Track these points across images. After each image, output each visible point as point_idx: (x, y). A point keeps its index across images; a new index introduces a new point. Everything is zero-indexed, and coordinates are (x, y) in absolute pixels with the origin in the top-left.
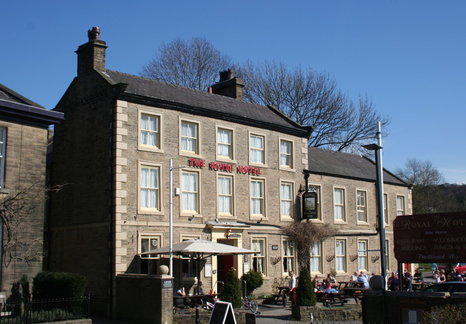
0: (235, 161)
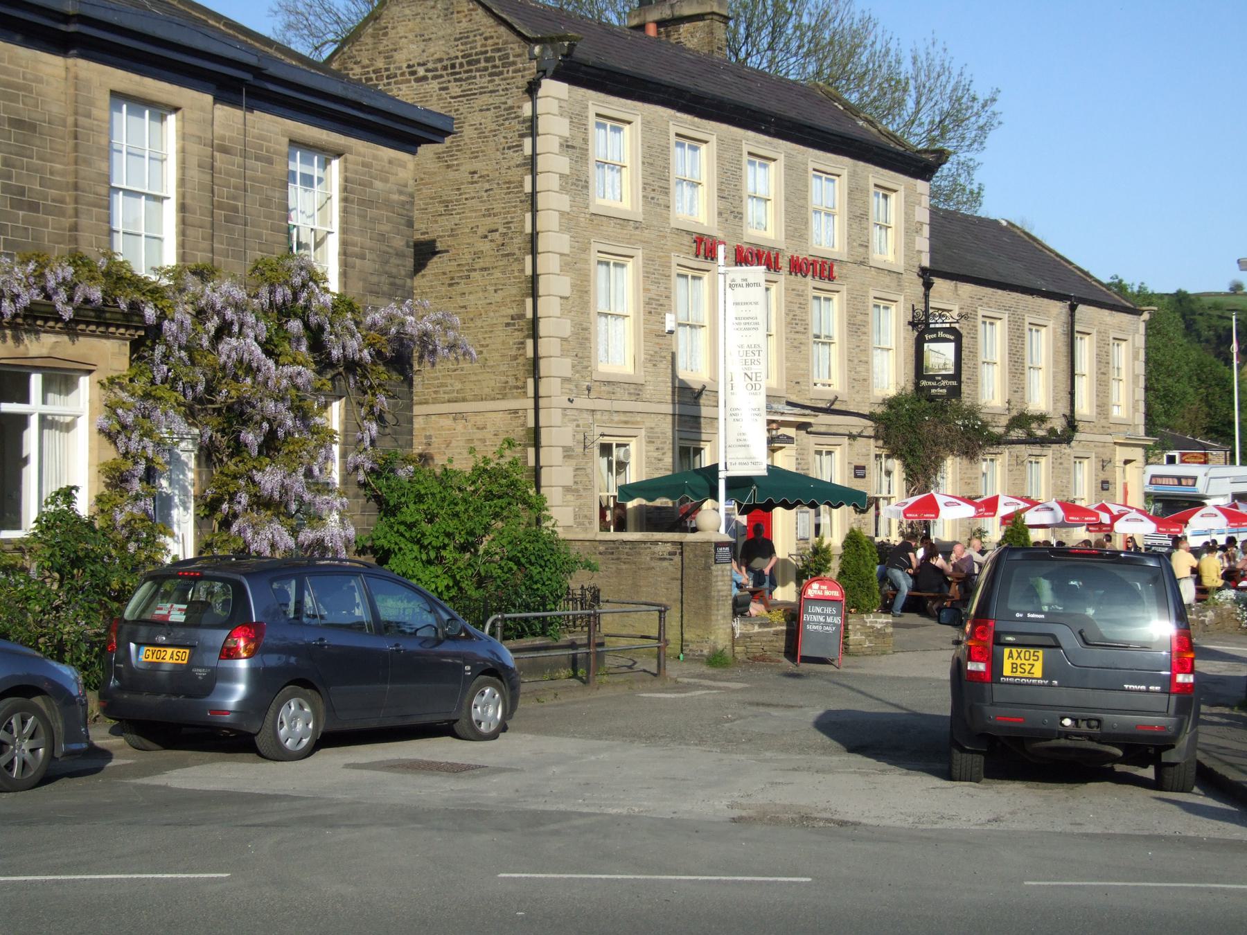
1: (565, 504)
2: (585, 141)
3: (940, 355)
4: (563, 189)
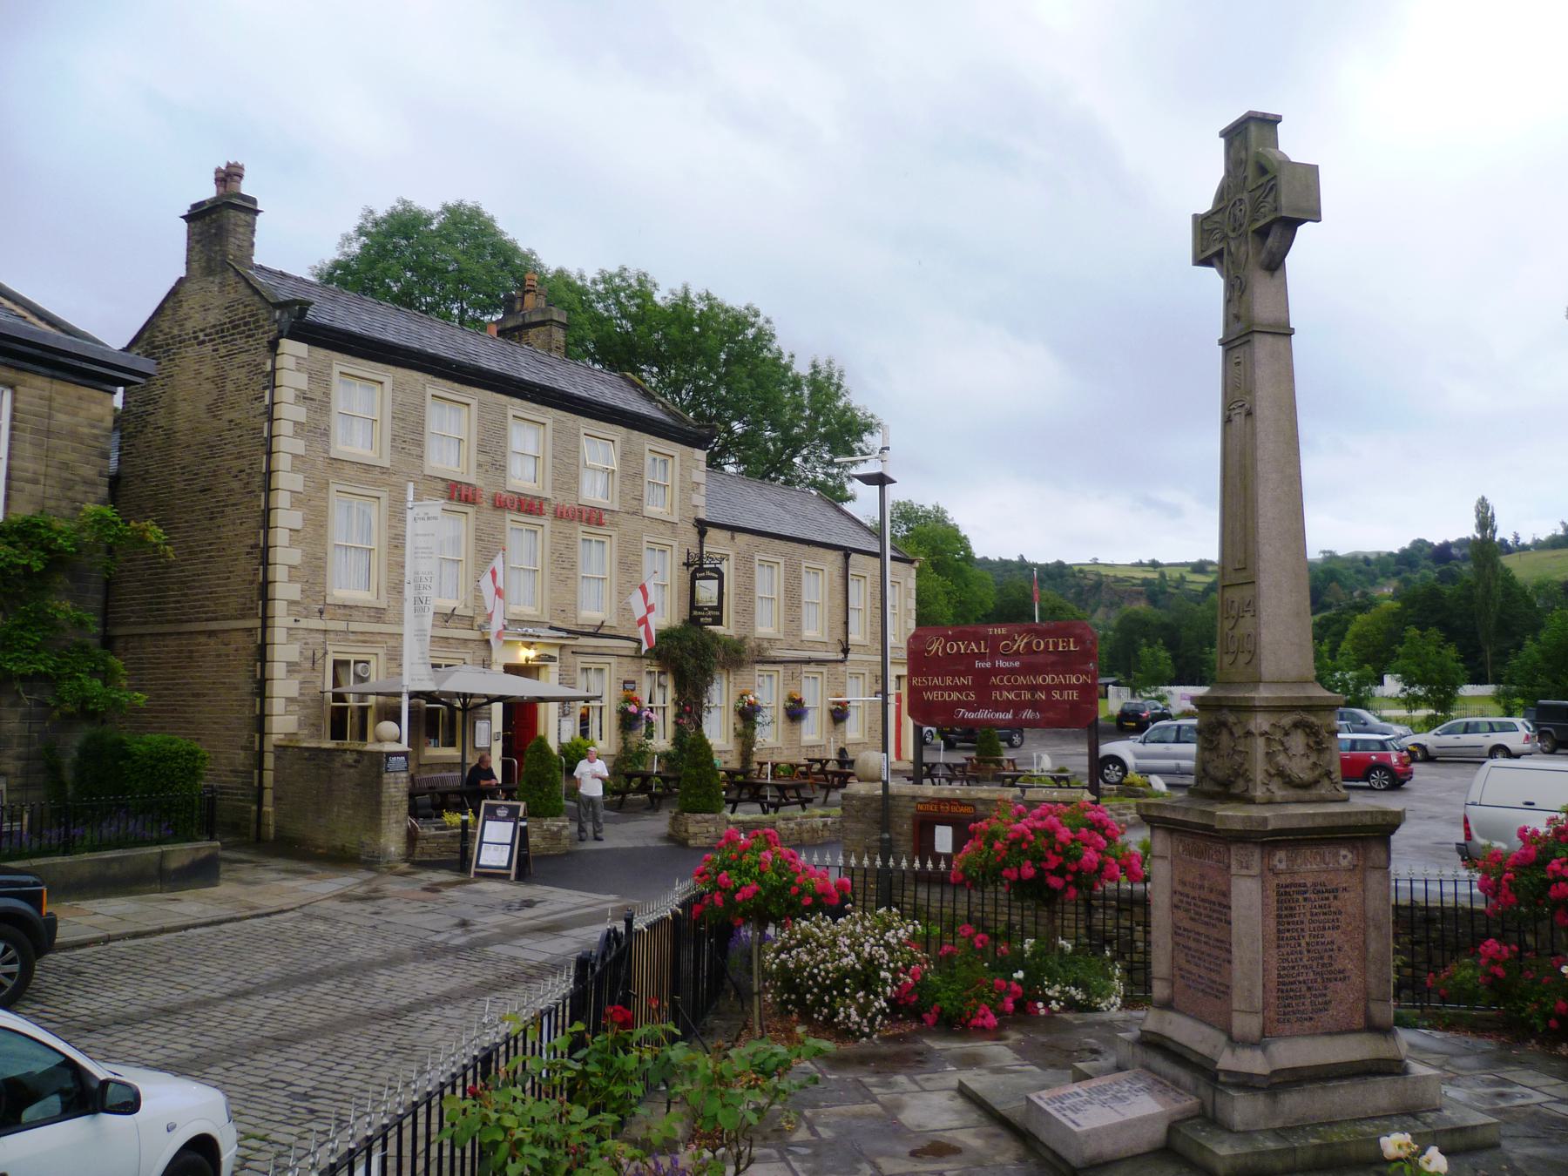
0: (548, 494)
1: (287, 713)
2: (327, 395)
3: (707, 591)
4: (296, 435)
